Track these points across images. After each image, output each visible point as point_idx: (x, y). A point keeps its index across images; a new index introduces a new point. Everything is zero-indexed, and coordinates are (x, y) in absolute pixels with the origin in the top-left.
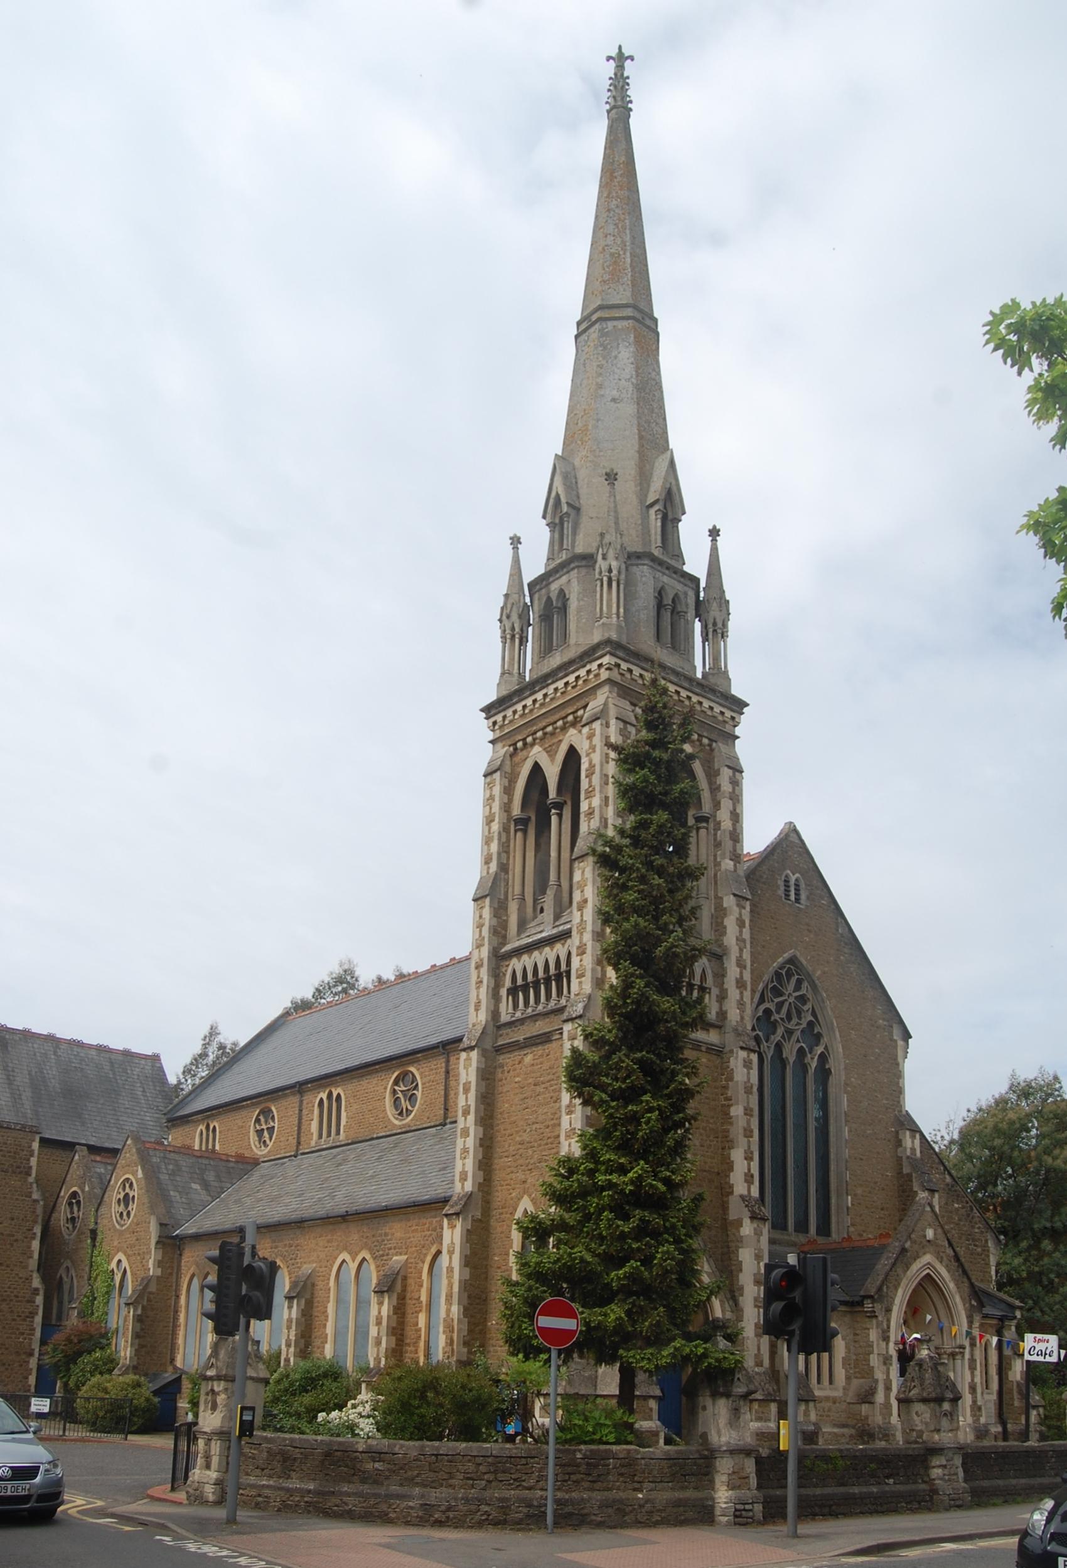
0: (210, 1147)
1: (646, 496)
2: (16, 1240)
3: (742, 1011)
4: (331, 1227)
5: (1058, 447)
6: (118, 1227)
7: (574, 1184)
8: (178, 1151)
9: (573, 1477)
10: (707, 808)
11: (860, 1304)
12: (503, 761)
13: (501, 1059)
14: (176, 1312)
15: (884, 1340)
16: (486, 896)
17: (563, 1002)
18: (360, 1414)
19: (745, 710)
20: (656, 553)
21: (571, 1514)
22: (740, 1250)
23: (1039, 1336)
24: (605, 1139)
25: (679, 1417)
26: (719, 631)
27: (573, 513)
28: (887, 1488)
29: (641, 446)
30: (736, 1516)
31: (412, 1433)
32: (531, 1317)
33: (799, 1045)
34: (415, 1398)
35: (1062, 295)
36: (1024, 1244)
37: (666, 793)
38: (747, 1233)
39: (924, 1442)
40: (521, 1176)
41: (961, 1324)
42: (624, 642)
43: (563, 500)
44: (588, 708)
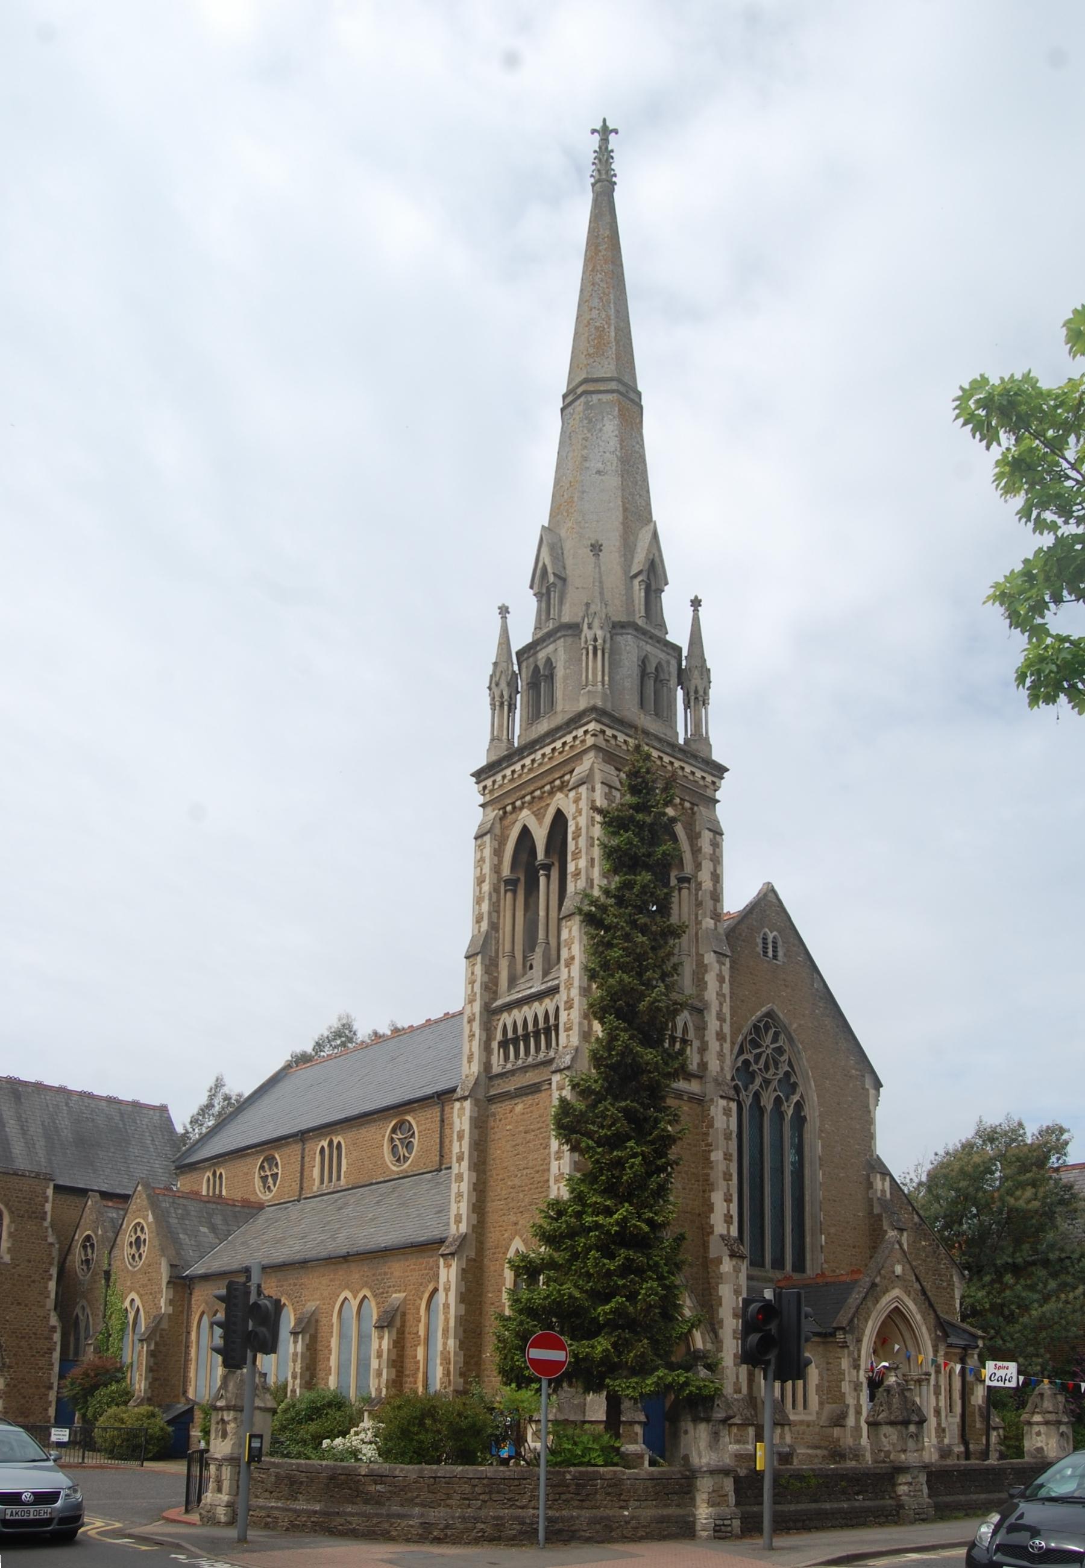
0: (217, 1192)
1: (630, 566)
2: (34, 1281)
3: (722, 1062)
5: (1024, 520)
7: (562, 1225)
9: (563, 1497)
10: (689, 869)
11: (833, 1335)
13: (493, 1108)
14: (187, 1347)
15: (855, 1368)
16: (477, 954)
17: (552, 1054)
18: (362, 1440)
19: (726, 775)
20: (640, 622)
21: (560, 1531)
22: (720, 1286)
23: (999, 1363)
25: (663, 1440)
26: (701, 699)
27: (559, 584)
28: (857, 1504)
29: (625, 518)
30: (715, 1531)
31: (411, 1458)
32: (523, 1350)
33: (776, 1094)
34: (414, 1425)
35: (1030, 371)
36: (987, 1279)
39: (891, 1461)
40: (513, 1218)
41: (927, 1353)
42: (609, 708)
43: (550, 570)
44: (575, 773)
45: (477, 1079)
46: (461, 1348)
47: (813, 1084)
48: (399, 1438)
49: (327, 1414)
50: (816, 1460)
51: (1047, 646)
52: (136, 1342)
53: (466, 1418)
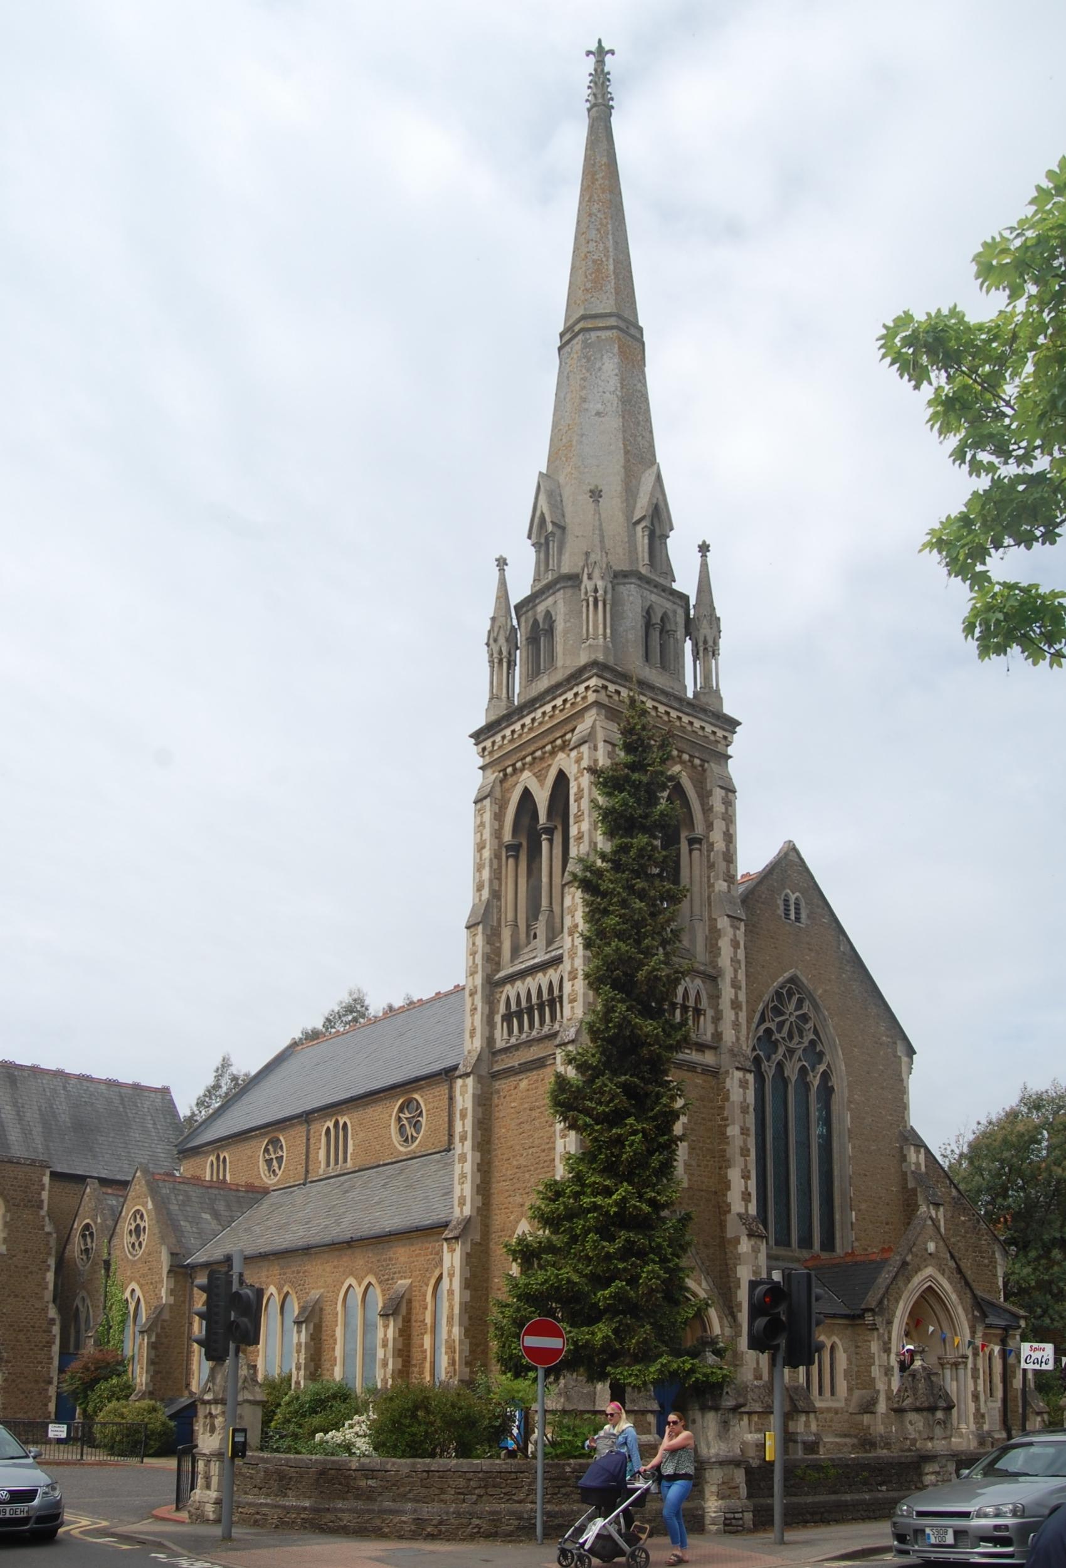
1: (633, 512)
2: (31, 1273)
3: (738, 1031)
4: (337, 1253)
6: (130, 1257)
7: (559, 1206)
8: (185, 1181)
9: (563, 1490)
10: (700, 829)
11: (861, 1317)
12: (493, 787)
13: (497, 1085)
15: (885, 1351)
16: (478, 924)
17: (556, 1027)
18: (356, 1433)
19: (738, 729)
22: (738, 1267)
23: (1035, 1345)
24: (591, 1162)
27: (558, 532)
28: (880, 1495)
29: (627, 461)
30: (725, 1525)
31: (404, 1451)
32: (518, 1336)
33: (800, 1064)
34: (406, 1417)
35: (955, 306)
36: (1033, 1254)
37: (646, 816)
38: (745, 1250)
39: (917, 1450)
40: (518, 1199)
42: (611, 663)
43: (548, 519)
44: (576, 732)
45: (480, 1055)
46: (466, 1336)
47: (840, 1052)
48: (391, 1431)
49: (331, 1406)
50: (845, 1450)
51: (995, 594)
52: (137, 1334)
53: (460, 1409)
